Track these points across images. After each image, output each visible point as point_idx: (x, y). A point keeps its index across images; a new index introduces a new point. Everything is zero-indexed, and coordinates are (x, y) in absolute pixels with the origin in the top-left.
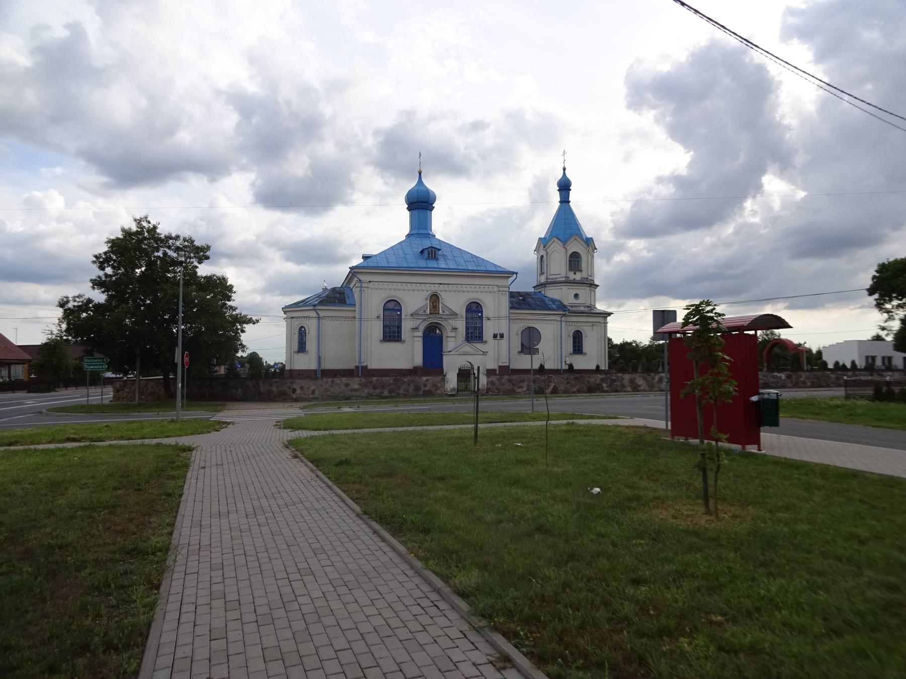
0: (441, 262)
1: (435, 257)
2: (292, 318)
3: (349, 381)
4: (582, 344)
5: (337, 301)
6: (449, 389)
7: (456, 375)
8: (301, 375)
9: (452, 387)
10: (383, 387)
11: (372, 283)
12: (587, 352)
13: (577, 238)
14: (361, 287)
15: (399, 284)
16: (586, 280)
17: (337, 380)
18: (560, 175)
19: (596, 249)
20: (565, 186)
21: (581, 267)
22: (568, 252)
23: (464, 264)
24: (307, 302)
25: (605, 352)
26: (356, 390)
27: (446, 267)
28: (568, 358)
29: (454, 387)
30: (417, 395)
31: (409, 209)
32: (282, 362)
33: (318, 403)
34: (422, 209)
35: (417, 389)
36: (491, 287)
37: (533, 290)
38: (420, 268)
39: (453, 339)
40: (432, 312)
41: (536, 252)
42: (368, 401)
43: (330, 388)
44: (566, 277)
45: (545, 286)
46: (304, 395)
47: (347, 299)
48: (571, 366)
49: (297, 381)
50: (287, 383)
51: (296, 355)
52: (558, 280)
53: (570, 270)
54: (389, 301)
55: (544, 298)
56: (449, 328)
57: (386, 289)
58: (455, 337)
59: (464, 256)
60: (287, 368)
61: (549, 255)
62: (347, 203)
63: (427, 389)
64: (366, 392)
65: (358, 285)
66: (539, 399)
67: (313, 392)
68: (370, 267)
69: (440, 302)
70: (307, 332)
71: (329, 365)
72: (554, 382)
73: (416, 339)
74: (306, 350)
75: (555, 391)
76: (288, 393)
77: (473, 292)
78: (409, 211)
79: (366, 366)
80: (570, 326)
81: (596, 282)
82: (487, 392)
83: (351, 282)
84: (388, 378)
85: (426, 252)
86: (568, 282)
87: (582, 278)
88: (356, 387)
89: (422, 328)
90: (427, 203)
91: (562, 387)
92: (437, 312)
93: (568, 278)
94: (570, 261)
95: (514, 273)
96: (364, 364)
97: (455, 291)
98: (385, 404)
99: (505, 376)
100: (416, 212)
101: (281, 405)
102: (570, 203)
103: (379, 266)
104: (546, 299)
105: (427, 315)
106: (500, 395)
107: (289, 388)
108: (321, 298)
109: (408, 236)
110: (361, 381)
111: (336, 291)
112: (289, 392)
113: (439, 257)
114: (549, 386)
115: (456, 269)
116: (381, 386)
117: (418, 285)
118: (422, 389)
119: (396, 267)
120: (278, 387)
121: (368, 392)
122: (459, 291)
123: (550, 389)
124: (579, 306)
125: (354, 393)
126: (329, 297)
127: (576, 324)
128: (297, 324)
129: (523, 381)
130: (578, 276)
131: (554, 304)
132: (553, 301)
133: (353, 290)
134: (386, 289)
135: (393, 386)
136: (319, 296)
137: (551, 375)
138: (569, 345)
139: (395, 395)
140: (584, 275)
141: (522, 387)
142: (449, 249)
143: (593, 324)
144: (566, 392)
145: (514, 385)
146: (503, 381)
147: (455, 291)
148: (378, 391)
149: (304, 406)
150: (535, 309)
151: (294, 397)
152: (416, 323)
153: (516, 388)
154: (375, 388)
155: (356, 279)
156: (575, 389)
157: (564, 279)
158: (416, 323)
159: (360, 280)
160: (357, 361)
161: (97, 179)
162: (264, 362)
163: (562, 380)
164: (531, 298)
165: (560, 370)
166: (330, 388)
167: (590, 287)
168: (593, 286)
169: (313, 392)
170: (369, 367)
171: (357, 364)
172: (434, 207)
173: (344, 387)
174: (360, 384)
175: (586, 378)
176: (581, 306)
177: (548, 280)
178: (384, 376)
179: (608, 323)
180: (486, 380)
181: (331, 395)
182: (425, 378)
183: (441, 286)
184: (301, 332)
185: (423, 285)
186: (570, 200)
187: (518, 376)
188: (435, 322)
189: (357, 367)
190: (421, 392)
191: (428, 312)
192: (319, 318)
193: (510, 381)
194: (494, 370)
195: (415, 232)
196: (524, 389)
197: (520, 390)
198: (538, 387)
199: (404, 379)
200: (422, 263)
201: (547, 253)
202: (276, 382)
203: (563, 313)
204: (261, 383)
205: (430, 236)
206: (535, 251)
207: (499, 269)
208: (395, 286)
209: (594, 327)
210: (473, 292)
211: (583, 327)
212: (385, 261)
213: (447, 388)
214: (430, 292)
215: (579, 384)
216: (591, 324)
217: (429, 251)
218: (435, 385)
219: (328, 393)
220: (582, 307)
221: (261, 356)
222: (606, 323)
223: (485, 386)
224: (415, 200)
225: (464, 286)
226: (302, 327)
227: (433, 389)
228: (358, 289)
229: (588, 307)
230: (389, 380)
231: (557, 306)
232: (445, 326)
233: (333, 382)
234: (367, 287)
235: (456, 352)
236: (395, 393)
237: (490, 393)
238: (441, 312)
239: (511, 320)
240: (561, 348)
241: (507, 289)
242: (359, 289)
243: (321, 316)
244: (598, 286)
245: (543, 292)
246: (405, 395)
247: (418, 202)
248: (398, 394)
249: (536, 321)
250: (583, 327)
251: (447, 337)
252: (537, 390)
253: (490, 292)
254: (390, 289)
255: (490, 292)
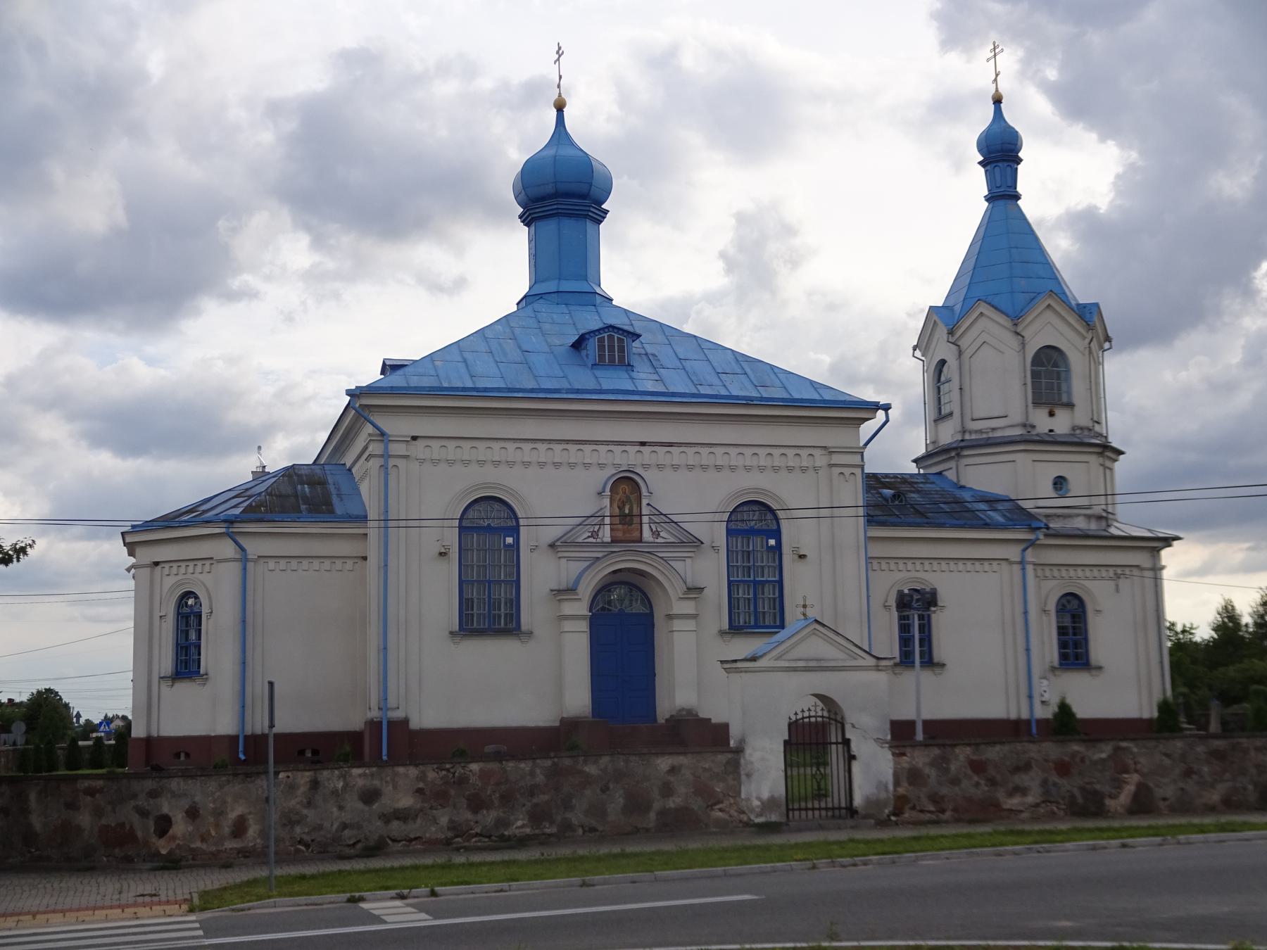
0: (642, 376)
1: (622, 358)
2: (156, 564)
3: (377, 783)
4: (1086, 640)
5: (303, 507)
6: (756, 803)
7: (781, 748)
8: (183, 757)
9: (765, 795)
10: (507, 799)
11: (420, 444)
12: (1102, 663)
13: (1053, 304)
14: (386, 456)
15: (511, 446)
16: (1086, 433)
17: (332, 779)
18: (983, 119)
19: (1108, 339)
20: (1002, 151)
21: (1069, 393)
22: (1027, 347)
23: (716, 381)
24: (205, 512)
25: (1161, 662)
26: (403, 816)
27: (661, 388)
28: (1045, 682)
29: (776, 795)
30: (637, 830)
31: (527, 219)
32: (126, 714)
33: (261, 873)
34: (570, 216)
35: (636, 804)
36: (804, 453)
37: (912, 469)
38: (578, 391)
39: (690, 625)
40: (619, 534)
41: (918, 353)
42: (460, 859)
43: (305, 812)
44: (1024, 425)
45: (958, 455)
46: (203, 840)
47: (335, 499)
48: (1064, 709)
49: (175, 784)
50: (134, 796)
51: (165, 689)
52: (998, 434)
53: (1037, 403)
54: (476, 501)
55: (959, 493)
56: (674, 589)
57: (466, 463)
58: (694, 617)
59: (710, 357)
60: (138, 732)
61: (966, 355)
62: (232, 296)
63: (672, 803)
64: (444, 820)
65: (375, 448)
66: (1129, 841)
67: (239, 829)
68: (416, 388)
69: (644, 502)
70: (205, 610)
71: (290, 721)
72: (1136, 771)
73: (568, 626)
74: (202, 671)
75: (1142, 804)
76: (139, 834)
77: (748, 469)
78: (528, 225)
79: (405, 722)
80: (1046, 578)
81: (1115, 443)
82: (897, 812)
83: (348, 446)
84: (525, 766)
85: (592, 344)
86: (1031, 440)
87: (1074, 429)
88: (406, 801)
89: (587, 589)
90: (584, 196)
91: (1167, 789)
92: (637, 534)
93: (1033, 427)
94: (1035, 375)
95: (875, 407)
96: (398, 715)
97: (690, 468)
98: (537, 877)
99: (957, 750)
100: (550, 227)
101: (107, 887)
102: (1020, 202)
103: (445, 385)
104: (967, 496)
105: (604, 544)
106: (947, 822)
107: (143, 813)
108: (250, 497)
109: (526, 300)
110: (422, 777)
111: (299, 476)
112: (144, 829)
113: (635, 361)
114: (1119, 784)
115: (693, 395)
116: (502, 797)
117: (573, 448)
118: (657, 806)
119: (499, 390)
120: (98, 812)
121: (451, 821)
122: (704, 468)
123: (1125, 797)
124: (1070, 516)
125: (396, 827)
126: (280, 496)
127: (1088, 573)
128: (170, 584)
129: (1026, 767)
130: (1061, 423)
131: (995, 510)
132: (992, 501)
133: (354, 471)
134: (466, 463)
135: (545, 797)
136: (242, 492)
137: (1124, 744)
138: (1047, 647)
139: (554, 830)
140: (1081, 417)
141: (1021, 790)
142: (661, 338)
143: (1119, 571)
144: (1183, 806)
145: (992, 782)
146: (953, 767)
147: (690, 468)
148: (489, 817)
149: (204, 895)
150: (941, 526)
151: (164, 852)
152: (563, 570)
153: (1000, 795)
154: (477, 804)
155: (369, 429)
156: (1215, 797)
157: (1018, 432)
158: (563, 570)
159: (383, 434)
160: (374, 702)
161: (365, 897)
162: (75, 713)
163: (1167, 762)
164: (918, 492)
165: (256, 743)
166: (305, 812)
167: (1101, 454)
168: (1108, 452)
169: (239, 829)
170: (415, 724)
171: (374, 714)
172: (606, 212)
173: (360, 805)
174: (419, 791)
175: (1253, 753)
176: (1078, 515)
177: (967, 437)
178: (513, 757)
179: (1163, 568)
180: (891, 764)
181: (307, 838)
182: (664, 763)
183: (646, 449)
184: (186, 610)
185: (587, 448)
186: (1019, 189)
187: (1006, 748)
188: (629, 570)
189: (374, 725)
190: (652, 815)
191: (606, 534)
192: (244, 559)
193: (978, 767)
194: (911, 724)
195: (551, 286)
196: (1030, 799)
197: (1014, 802)
198: (1082, 789)
199: (587, 769)
200: (583, 378)
201: (960, 353)
202: (91, 792)
203: (1031, 536)
204: (33, 797)
205: (595, 298)
206: (915, 348)
207: (827, 396)
208: (496, 452)
209: (1123, 583)
210: (748, 469)
211: (1086, 583)
212: (463, 370)
213: (748, 799)
214: (610, 471)
215: (1227, 776)
216: (1111, 571)
217: (601, 340)
218: (703, 790)
219: (298, 830)
220: (1081, 519)
221: (65, 700)
222: (1157, 569)
223: (887, 790)
224: (550, 189)
225: (719, 451)
226: (188, 594)
227: (697, 804)
228: (375, 464)
229: (1099, 518)
230: (532, 774)
231: (1004, 516)
232: (666, 584)
233: (315, 785)
234: (406, 457)
235: (778, 658)
236: (552, 822)
237: (906, 815)
238: (647, 535)
239: (875, 562)
240: (1028, 650)
241: (856, 459)
242: (380, 461)
243: (250, 557)
244: (1122, 453)
245: (951, 475)
246: (593, 830)
247: (557, 195)
248: (567, 827)
249: (944, 565)
250: (1086, 583)
251: (670, 617)
252: (1080, 800)
253: (804, 470)
254: (481, 463)
255: (804, 470)
